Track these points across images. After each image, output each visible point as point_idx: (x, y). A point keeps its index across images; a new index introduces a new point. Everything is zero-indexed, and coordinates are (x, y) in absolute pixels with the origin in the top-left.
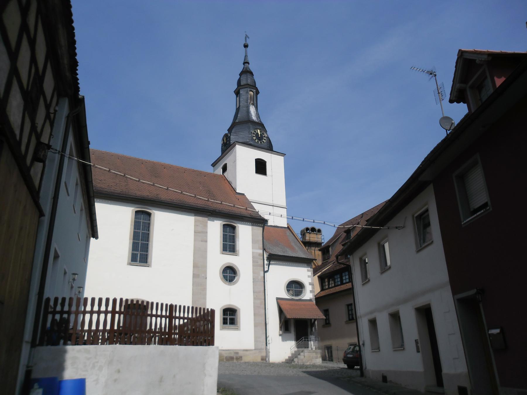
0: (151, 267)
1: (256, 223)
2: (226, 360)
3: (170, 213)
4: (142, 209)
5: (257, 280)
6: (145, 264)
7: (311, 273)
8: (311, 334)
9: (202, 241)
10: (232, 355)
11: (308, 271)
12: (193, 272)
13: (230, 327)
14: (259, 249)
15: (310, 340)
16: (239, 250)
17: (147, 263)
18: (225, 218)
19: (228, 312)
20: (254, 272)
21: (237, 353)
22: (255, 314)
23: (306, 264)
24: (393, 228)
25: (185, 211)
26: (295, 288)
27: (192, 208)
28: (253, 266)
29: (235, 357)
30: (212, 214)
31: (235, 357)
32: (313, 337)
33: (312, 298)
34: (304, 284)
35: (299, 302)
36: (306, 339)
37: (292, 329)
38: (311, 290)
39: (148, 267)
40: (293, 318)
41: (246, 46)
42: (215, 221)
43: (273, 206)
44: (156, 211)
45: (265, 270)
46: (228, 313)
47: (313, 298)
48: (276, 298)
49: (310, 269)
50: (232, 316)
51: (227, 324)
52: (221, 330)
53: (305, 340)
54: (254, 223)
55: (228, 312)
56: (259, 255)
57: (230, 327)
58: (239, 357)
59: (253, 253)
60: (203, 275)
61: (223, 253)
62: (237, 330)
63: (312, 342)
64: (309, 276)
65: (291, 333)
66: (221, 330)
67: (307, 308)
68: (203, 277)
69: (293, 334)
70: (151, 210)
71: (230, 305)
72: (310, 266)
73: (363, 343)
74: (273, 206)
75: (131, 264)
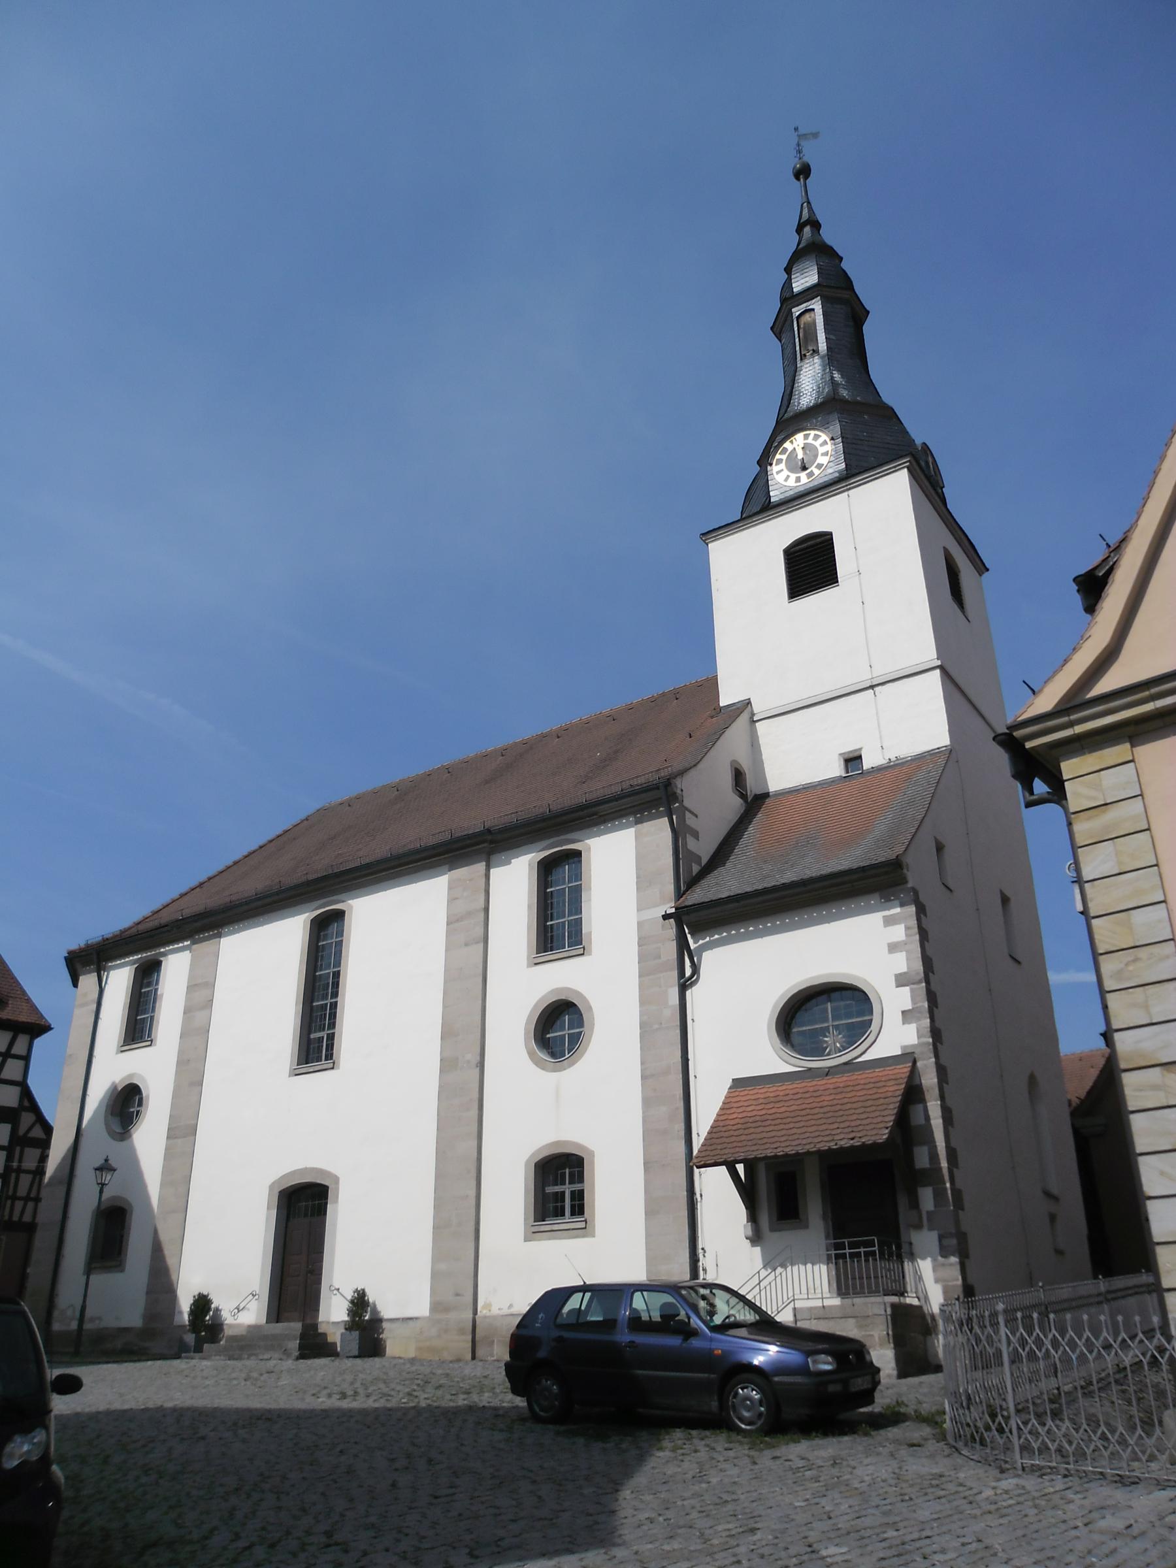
3: (388, 891)
4: (324, 908)
5: (656, 1026)
7: (907, 928)
8: (918, 1226)
9: (466, 945)
11: (888, 922)
13: (556, 1227)
15: (912, 1257)
18: (541, 839)
19: (567, 1171)
22: (647, 1165)
23: (877, 895)
25: (416, 870)
26: (826, 1020)
27: (423, 855)
30: (491, 842)
32: (926, 1239)
33: (913, 1046)
34: (796, 991)
35: (834, 1080)
36: (862, 1250)
37: (814, 1208)
38: (909, 1006)
39: (333, 1068)
40: (820, 1153)
41: (803, 172)
42: (513, 861)
43: (872, 687)
44: (355, 900)
46: (565, 1173)
47: (920, 1045)
49: (898, 910)
50: (561, 1184)
51: (563, 1215)
52: (527, 1239)
53: (858, 1255)
54: (642, 813)
55: (567, 1171)
57: (556, 1227)
62: (584, 1236)
63: (925, 1266)
64: (893, 948)
65: (806, 1227)
66: (527, 1239)
67: (854, 1100)
68: (469, 1062)
69: (815, 1232)
70: (343, 902)
71: (557, 1143)
72: (897, 898)
73: (966, 1261)
74: (872, 687)
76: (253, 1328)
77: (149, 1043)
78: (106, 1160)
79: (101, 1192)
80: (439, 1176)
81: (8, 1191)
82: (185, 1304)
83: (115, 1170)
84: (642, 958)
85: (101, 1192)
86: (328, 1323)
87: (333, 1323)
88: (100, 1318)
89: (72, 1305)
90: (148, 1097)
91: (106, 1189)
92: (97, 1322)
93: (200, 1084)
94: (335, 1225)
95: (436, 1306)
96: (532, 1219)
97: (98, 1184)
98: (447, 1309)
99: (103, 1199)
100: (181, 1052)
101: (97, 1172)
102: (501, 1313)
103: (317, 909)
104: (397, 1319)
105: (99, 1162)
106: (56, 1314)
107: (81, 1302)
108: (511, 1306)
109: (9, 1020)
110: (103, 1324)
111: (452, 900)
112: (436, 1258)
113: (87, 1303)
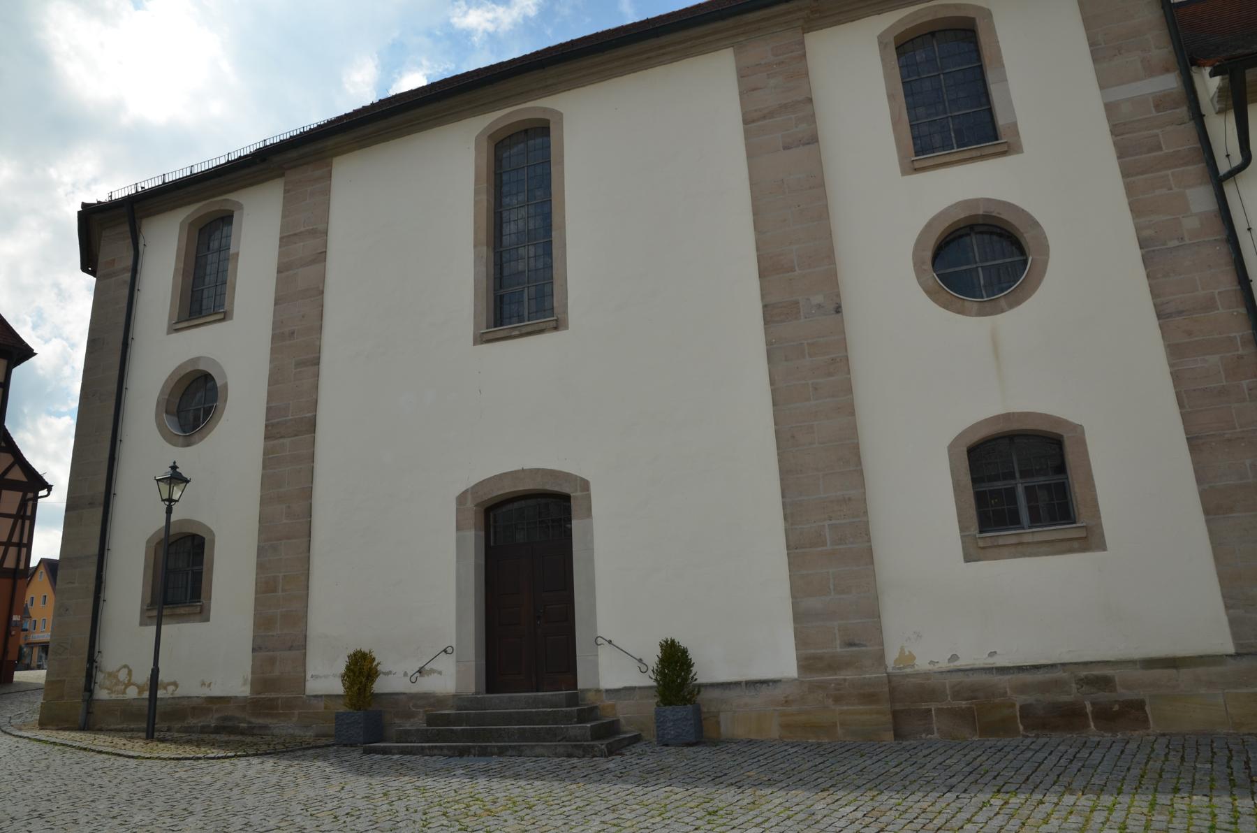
0: (566, 327)
1: (324, 124)
2: (1026, 728)
5: (1175, 243)
6: (988, 147)
9: (786, 147)
10: (1069, 696)
12: (763, 296)
14: (1150, 71)
16: (1014, 126)
17: (997, 139)
20: (1137, 209)
21: (1104, 683)
24: (951, 237)
28: (1125, 174)
29: (1089, 708)
31: (1089, 708)
45: (1223, 168)
48: (1102, 546)
52: (968, 558)
56: (1160, 102)
58: (1116, 708)
59: (1110, 108)
60: (818, 299)
61: (917, 165)
68: (819, 306)
75: (491, 336)
76: (459, 700)
77: (221, 316)
78: (174, 468)
79: (169, 511)
80: (788, 474)
81: (25, 511)
82: (907, 653)
83: (187, 481)
84: (1122, 152)
85: (169, 511)
86: (598, 691)
87: (607, 691)
88: (175, 684)
89: (125, 666)
90: (225, 386)
91: (175, 507)
92: (171, 688)
93: (316, 362)
94: (590, 549)
95: (807, 663)
96: (974, 528)
97: (163, 500)
98: (834, 665)
99: (172, 520)
100: (277, 324)
101: (160, 483)
102: (936, 668)
103: (534, 109)
104: (737, 684)
105: (165, 472)
106: (100, 677)
107: (151, 666)
108: (954, 658)
109: (240, 158)
110: (180, 692)
111: (746, 92)
112: (797, 593)
113: (160, 665)
